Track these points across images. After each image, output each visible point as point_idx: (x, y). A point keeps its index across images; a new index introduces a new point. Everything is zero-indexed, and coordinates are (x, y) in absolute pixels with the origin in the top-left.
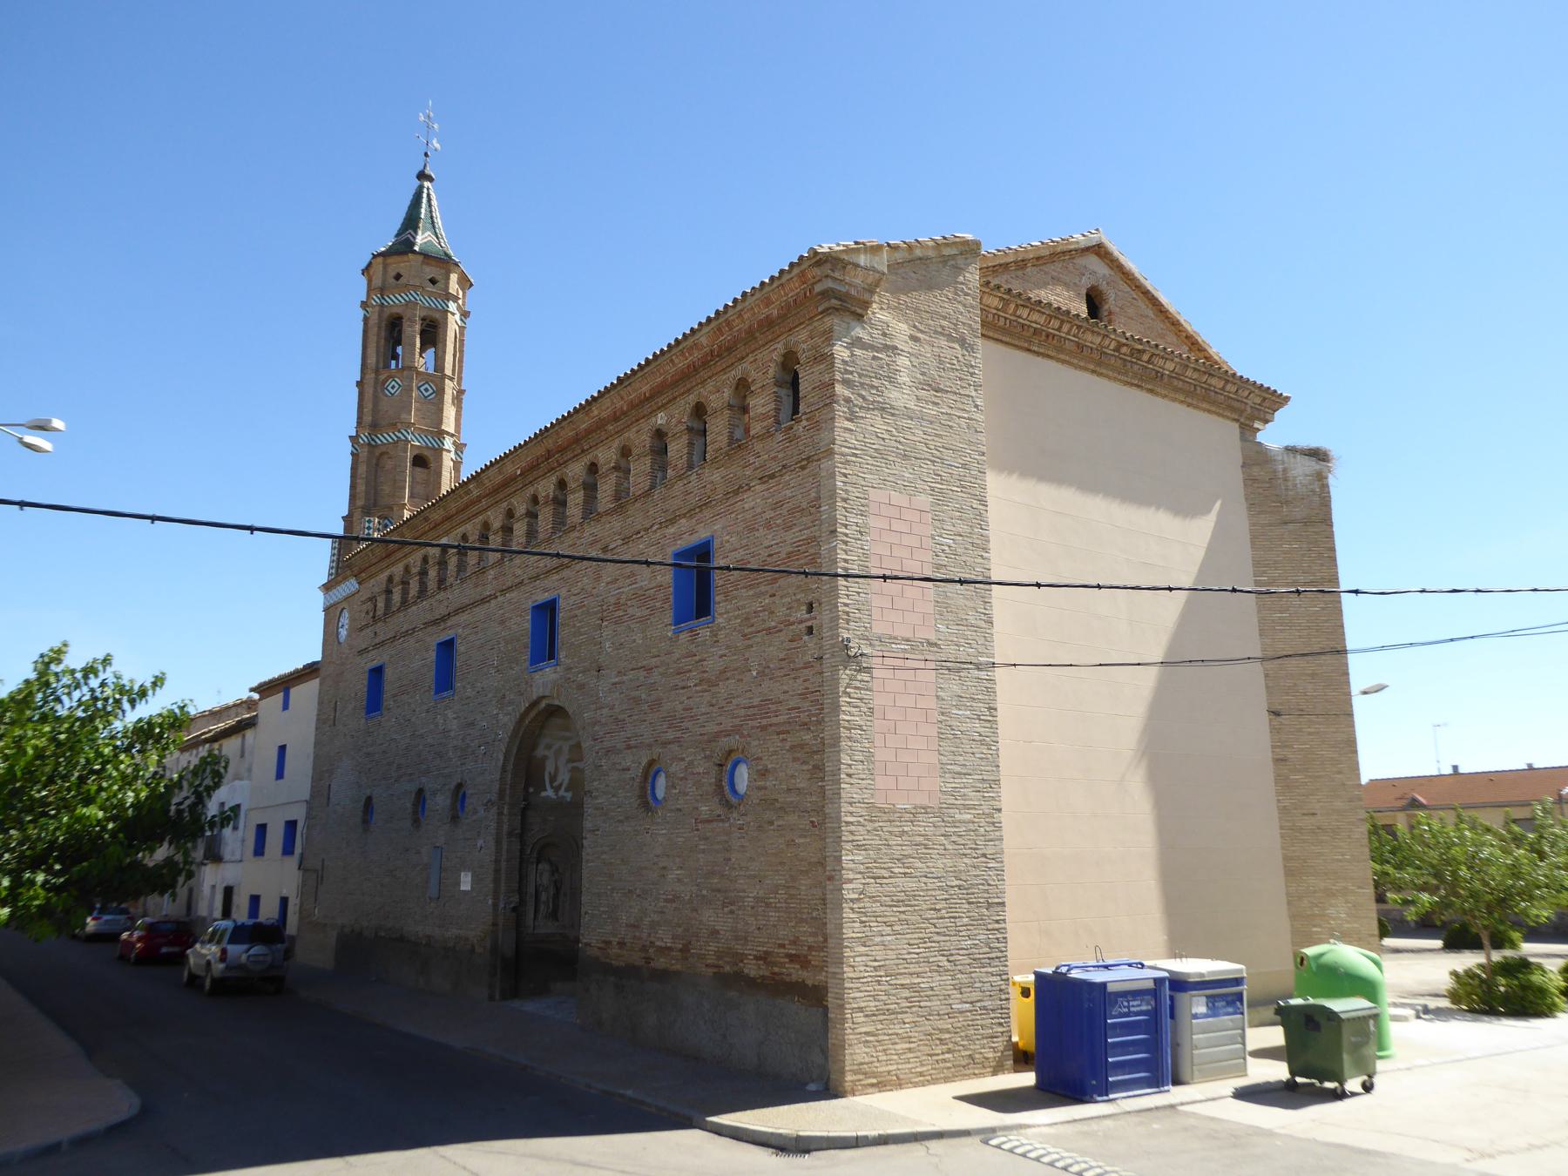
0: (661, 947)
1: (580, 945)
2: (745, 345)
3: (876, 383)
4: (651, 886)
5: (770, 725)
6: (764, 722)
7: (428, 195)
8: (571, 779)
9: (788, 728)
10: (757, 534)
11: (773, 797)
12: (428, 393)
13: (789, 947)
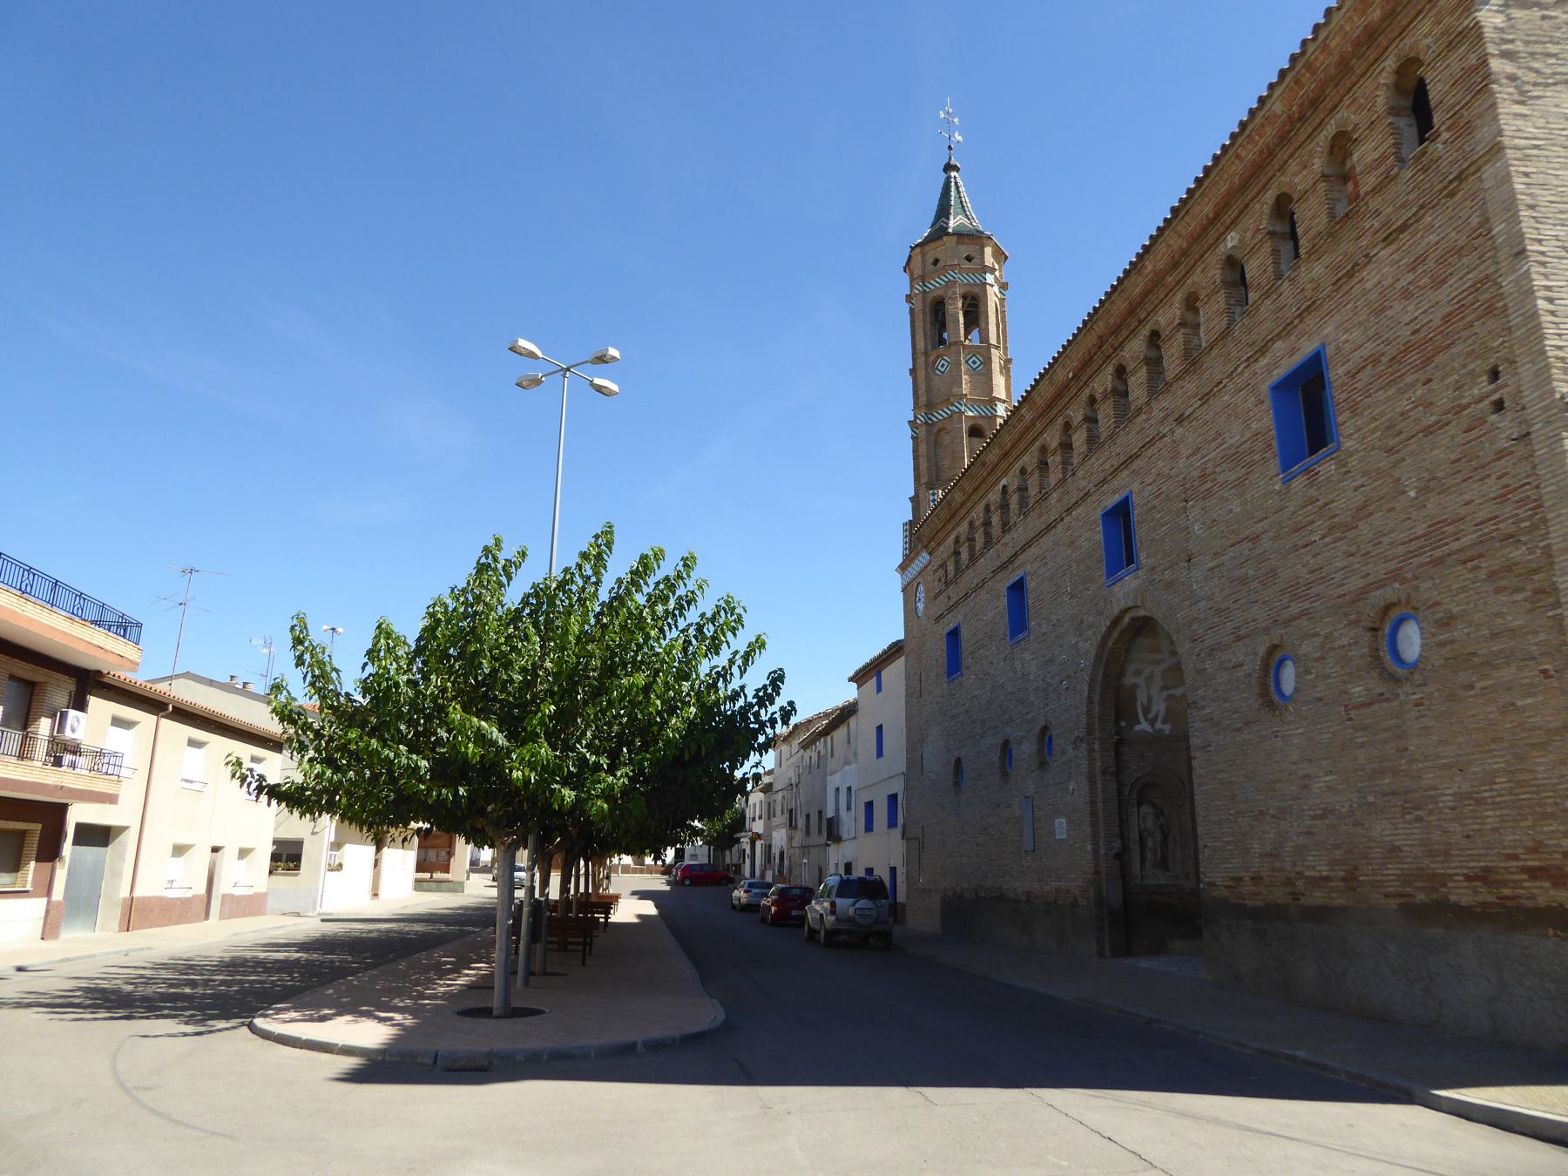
0: (1312, 878)
1: (1202, 886)
2: (1336, 86)
3: (1552, 49)
4: (1291, 803)
5: (1449, 555)
6: (1438, 553)
7: (956, 183)
8: (1168, 709)
9: (1479, 549)
10: (1389, 313)
11: (1469, 650)
13: (1526, 857)
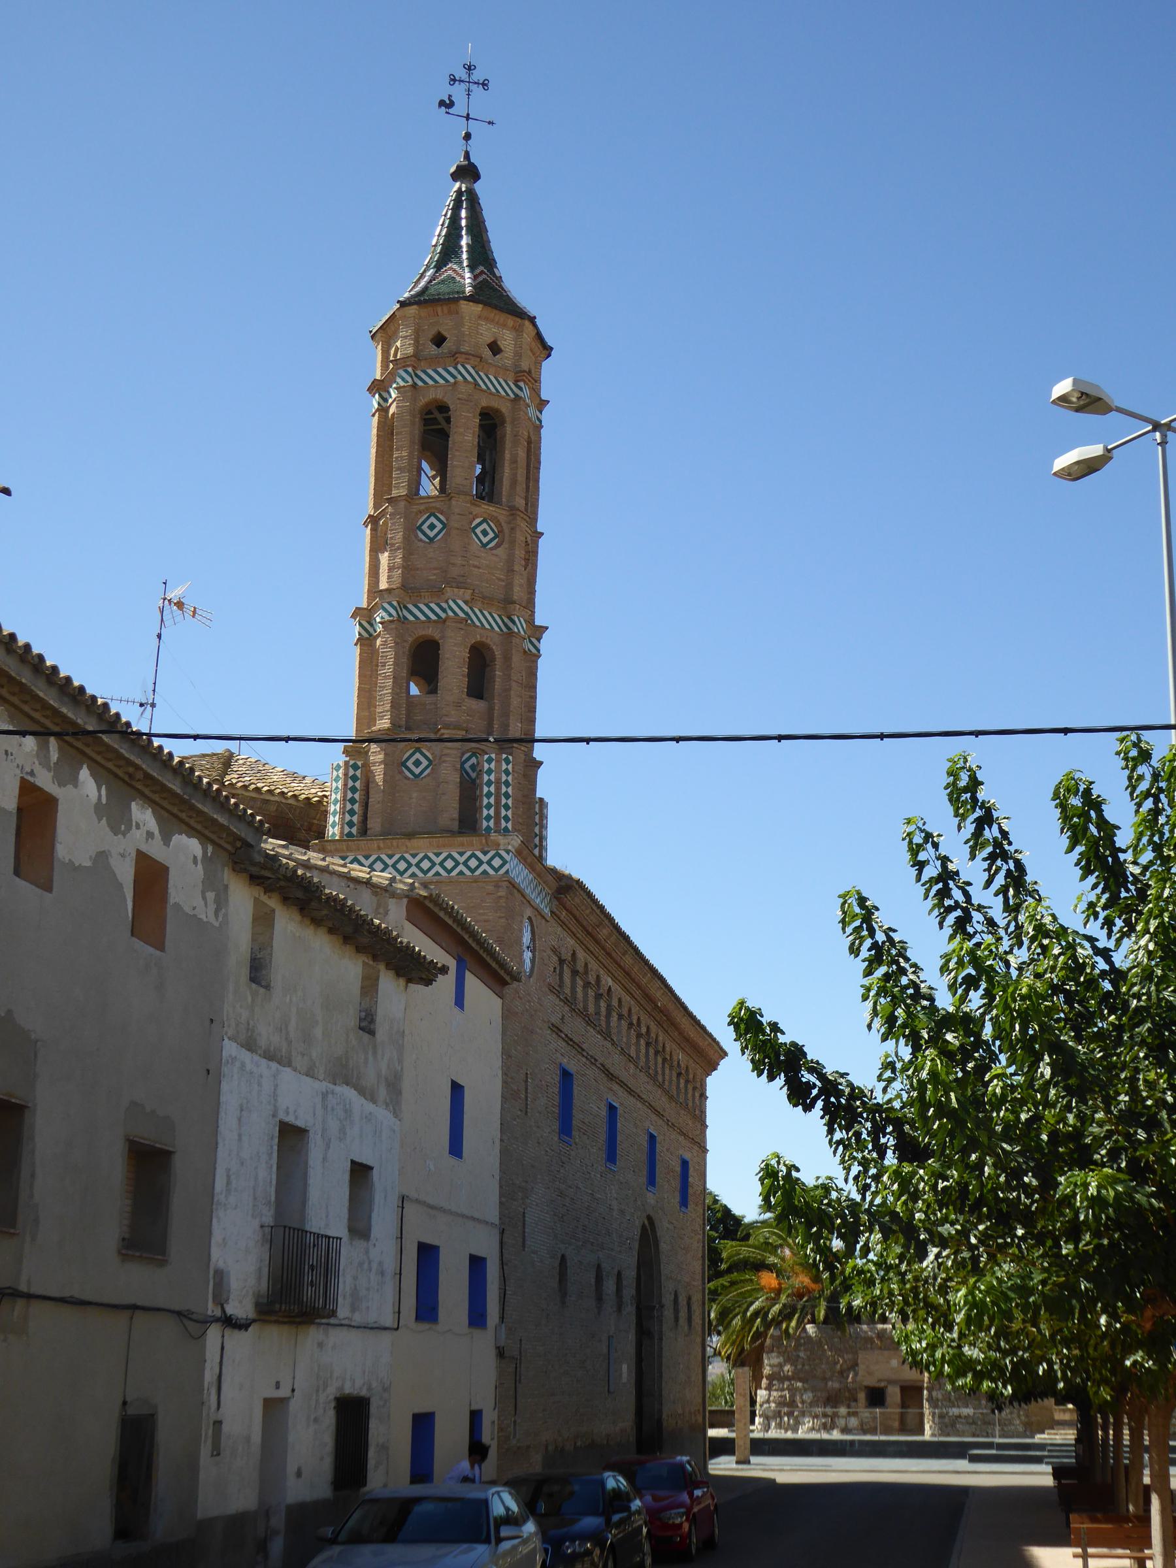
12: (422, 759)
